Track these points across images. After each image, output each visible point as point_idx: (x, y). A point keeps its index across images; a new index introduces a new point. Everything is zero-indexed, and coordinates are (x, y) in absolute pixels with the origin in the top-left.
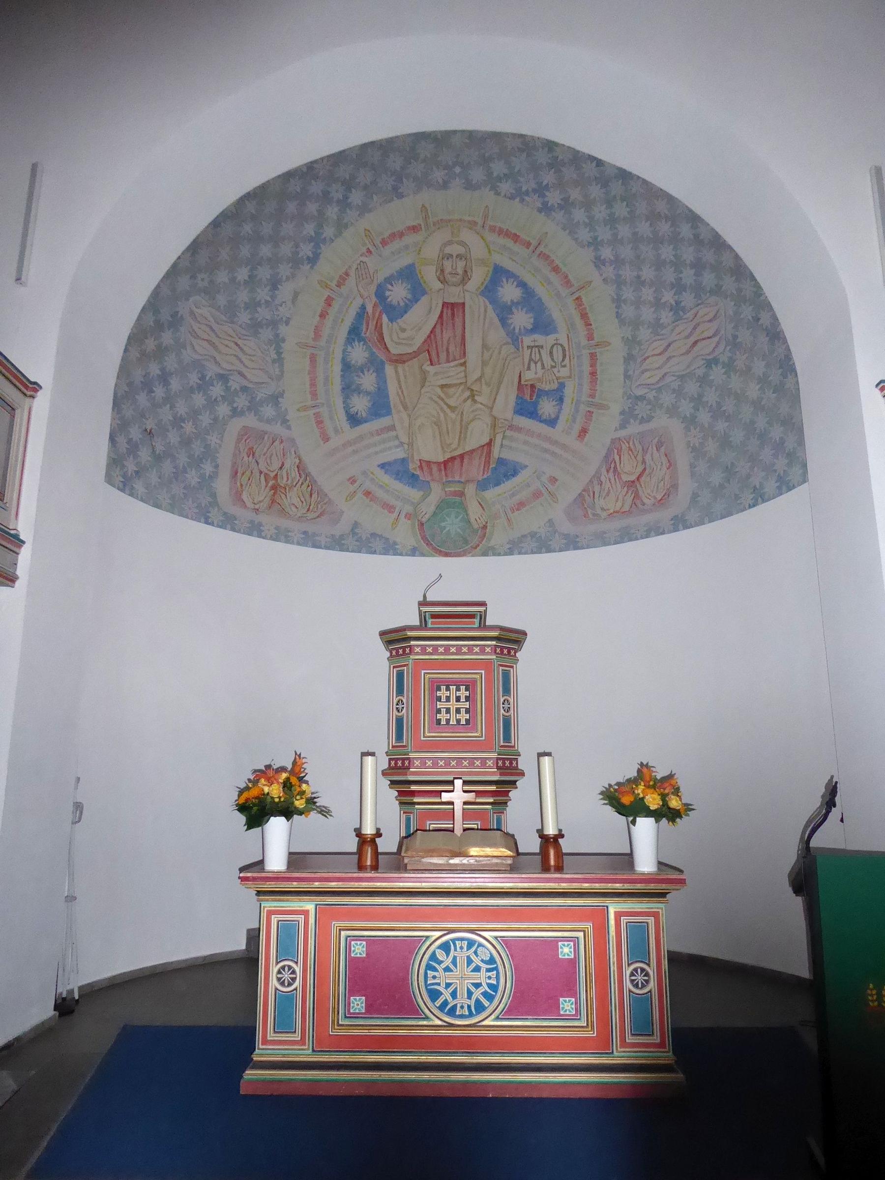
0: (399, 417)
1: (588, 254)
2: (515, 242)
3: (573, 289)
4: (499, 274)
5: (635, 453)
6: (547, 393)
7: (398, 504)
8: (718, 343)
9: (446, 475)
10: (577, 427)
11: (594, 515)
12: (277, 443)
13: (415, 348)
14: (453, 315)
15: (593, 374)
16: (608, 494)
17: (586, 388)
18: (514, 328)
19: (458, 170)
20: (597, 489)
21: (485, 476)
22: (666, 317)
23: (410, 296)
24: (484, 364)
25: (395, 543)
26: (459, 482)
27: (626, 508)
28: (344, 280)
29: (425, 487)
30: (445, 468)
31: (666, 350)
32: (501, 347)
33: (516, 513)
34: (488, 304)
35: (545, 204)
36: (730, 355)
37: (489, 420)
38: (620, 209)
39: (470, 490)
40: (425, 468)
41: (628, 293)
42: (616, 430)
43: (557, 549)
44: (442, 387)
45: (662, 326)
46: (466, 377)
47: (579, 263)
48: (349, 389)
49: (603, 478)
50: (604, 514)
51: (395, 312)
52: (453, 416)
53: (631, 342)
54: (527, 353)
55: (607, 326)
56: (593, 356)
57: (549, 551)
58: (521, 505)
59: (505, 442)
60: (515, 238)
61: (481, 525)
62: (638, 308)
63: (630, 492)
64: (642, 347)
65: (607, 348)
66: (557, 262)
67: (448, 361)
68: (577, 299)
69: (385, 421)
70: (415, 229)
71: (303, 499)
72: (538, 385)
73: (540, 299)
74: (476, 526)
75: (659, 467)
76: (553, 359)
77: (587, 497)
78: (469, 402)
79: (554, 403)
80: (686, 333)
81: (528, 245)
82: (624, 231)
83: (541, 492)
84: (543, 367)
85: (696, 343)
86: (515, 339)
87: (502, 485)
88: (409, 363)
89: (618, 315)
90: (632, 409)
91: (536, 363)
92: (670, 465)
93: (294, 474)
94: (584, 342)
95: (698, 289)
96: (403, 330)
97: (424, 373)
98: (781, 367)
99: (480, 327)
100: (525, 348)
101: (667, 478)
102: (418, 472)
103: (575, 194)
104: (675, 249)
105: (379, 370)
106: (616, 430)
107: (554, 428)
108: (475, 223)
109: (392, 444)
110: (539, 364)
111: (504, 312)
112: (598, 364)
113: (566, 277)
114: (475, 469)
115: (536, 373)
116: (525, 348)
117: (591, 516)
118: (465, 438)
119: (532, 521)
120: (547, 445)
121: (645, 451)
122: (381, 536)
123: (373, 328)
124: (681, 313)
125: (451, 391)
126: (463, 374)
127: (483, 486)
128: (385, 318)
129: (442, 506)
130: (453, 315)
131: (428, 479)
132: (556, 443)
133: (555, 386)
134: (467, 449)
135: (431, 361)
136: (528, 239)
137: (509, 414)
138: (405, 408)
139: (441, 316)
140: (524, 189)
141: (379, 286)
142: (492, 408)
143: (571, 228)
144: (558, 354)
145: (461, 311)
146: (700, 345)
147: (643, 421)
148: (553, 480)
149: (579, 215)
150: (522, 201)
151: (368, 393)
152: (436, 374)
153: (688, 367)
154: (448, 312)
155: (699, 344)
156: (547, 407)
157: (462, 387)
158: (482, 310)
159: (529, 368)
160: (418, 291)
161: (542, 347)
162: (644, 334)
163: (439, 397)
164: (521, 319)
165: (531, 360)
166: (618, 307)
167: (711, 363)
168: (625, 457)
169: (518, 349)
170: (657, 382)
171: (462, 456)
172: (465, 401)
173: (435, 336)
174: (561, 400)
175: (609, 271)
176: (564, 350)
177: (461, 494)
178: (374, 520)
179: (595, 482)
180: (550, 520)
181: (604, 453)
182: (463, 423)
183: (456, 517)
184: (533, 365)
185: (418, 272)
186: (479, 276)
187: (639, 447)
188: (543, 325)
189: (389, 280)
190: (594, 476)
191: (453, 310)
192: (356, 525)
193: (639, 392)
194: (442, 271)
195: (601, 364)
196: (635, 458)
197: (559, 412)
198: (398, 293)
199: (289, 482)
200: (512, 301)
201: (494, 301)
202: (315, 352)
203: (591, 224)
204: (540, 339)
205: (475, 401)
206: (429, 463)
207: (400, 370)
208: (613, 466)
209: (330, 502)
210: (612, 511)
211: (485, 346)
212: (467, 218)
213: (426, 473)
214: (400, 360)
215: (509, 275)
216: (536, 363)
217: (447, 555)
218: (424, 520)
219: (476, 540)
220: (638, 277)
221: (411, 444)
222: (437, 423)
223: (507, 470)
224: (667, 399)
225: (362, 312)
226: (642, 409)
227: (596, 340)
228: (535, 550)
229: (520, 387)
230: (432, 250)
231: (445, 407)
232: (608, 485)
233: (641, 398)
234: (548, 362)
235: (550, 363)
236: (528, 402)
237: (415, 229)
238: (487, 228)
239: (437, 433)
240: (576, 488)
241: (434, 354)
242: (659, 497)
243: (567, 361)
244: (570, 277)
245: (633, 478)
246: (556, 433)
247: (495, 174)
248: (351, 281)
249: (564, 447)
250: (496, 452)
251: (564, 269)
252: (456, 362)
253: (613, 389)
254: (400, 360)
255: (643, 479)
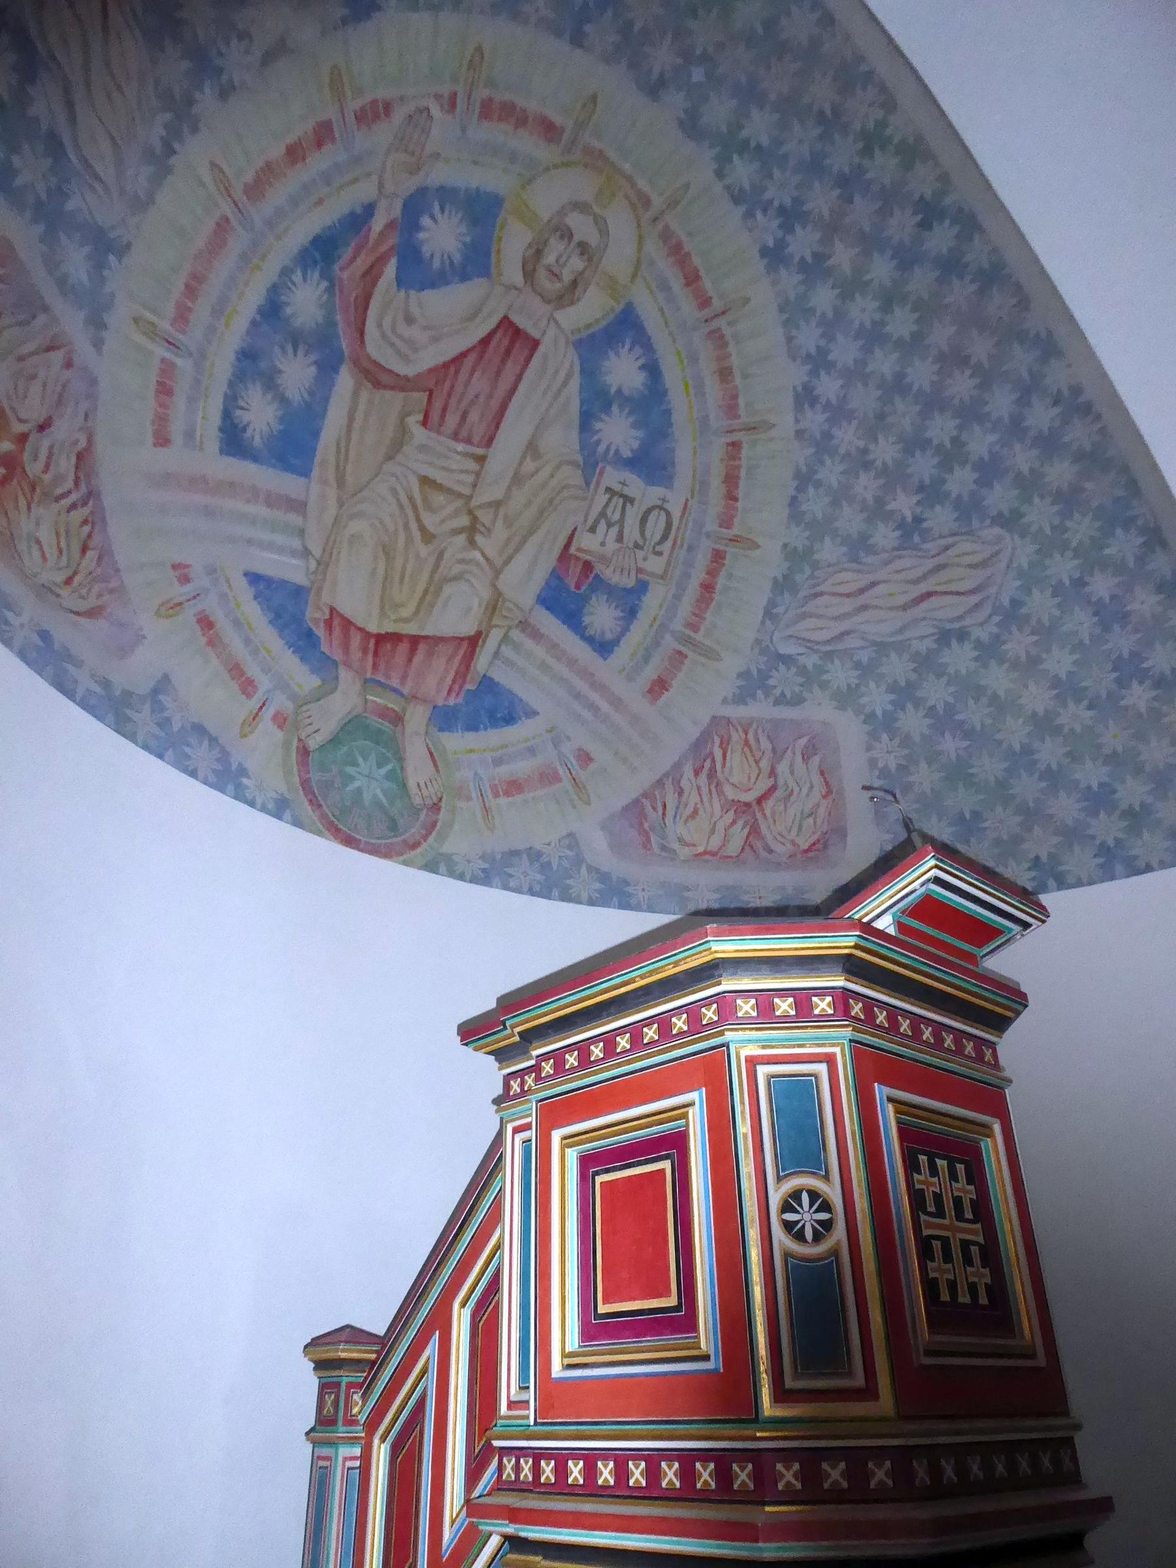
0: (316, 489)
1: (797, 375)
2: (688, 284)
3: (736, 423)
4: (625, 326)
5: (758, 754)
6: (612, 592)
7: (264, 683)
8: (977, 606)
9: (375, 666)
10: (650, 673)
11: (663, 848)
12: (57, 357)
13: (409, 371)
14: (508, 352)
15: (708, 588)
16: (695, 812)
17: (685, 609)
18: (598, 442)
19: (698, 74)
20: (671, 800)
21: (451, 702)
22: (885, 536)
23: (457, 258)
24: (517, 479)
25: (242, 771)
26: (395, 690)
27: (734, 847)
28: (376, 117)
29: (325, 666)
30: (376, 654)
31: (862, 591)
32: (558, 467)
33: (503, 801)
34: (577, 368)
35: (781, 245)
36: (995, 630)
37: (486, 594)
38: (901, 323)
39: (417, 717)
40: (337, 631)
41: (831, 473)
42: (725, 701)
43: (584, 896)
44: (425, 481)
45: (872, 550)
46: (474, 486)
47: (771, 383)
48: (251, 364)
49: (685, 784)
50: (684, 852)
51: (418, 272)
52: (424, 550)
53: (796, 557)
54: (603, 498)
55: (765, 516)
56: (718, 557)
57: (566, 897)
58: (514, 787)
59: (506, 651)
60: (692, 279)
61: (429, 802)
62: (835, 503)
63: (740, 823)
64: (817, 573)
65: (749, 552)
66: (735, 361)
67: (455, 436)
68: (733, 444)
69: (287, 484)
70: (549, 130)
71: (63, 545)
72: (599, 568)
73: (668, 413)
74: (417, 801)
75: (805, 790)
76: (642, 533)
77: (649, 809)
78: (461, 539)
79: (619, 614)
80: (913, 575)
81: (705, 302)
82: (884, 363)
83: (556, 772)
84: (620, 538)
85: (929, 594)
86: (591, 462)
87: (482, 733)
88: (388, 394)
89: (793, 502)
90: (764, 676)
91: (610, 525)
92: (829, 792)
93: (65, 465)
94: (711, 526)
95: (969, 510)
96: (410, 320)
97: (403, 431)
98: (1115, 669)
99: (542, 403)
100: (602, 489)
101: (822, 811)
102: (320, 632)
103: (843, 256)
104: (960, 428)
105: (328, 369)
106: (725, 701)
107: (605, 659)
108: (647, 203)
109: (279, 539)
110: (614, 531)
111: (597, 402)
112: (723, 573)
113: (735, 397)
114: (434, 677)
115: (603, 544)
116: (602, 489)
117: (656, 850)
118: (432, 605)
119: (535, 823)
120: (581, 685)
121: (778, 754)
122: (213, 740)
123: (363, 269)
124: (916, 539)
125: (439, 499)
126: (470, 479)
127: (444, 719)
128: (390, 270)
129: (352, 727)
130: (508, 352)
131: (338, 655)
132: (601, 688)
133: (630, 582)
134: (428, 631)
135: (426, 416)
136: (711, 293)
137: (527, 598)
138: (341, 482)
139: (485, 341)
140: (767, 195)
141: (422, 191)
142: (498, 573)
143: (794, 312)
144: (656, 525)
145: (526, 352)
146: (934, 601)
147: (780, 701)
148: (585, 758)
149: (824, 298)
150: (749, 215)
151: (283, 400)
152: (423, 448)
153: (901, 631)
154: (501, 341)
155: (933, 599)
156: (602, 616)
157: (459, 503)
158: (562, 375)
159: (593, 530)
160: (477, 261)
161: (632, 501)
162: (828, 551)
163: (411, 499)
164: (619, 432)
165: (603, 514)
166: (799, 489)
167: (944, 637)
168: (735, 759)
169: (588, 484)
170: (828, 642)
171: (415, 641)
172: (457, 532)
173: (457, 373)
174: (631, 613)
175: (815, 420)
176: (669, 524)
177: (397, 719)
178: (204, 692)
179: (668, 784)
180: (570, 835)
181: (694, 733)
182: (437, 577)
183: (379, 766)
184: (602, 526)
185: (499, 220)
186: (591, 308)
187: (765, 744)
188: (651, 462)
189: (446, 194)
190: (666, 775)
191: (512, 341)
192: (164, 684)
193: (785, 649)
194: (539, 253)
195: (730, 576)
196: (757, 762)
197: (623, 634)
198: (442, 236)
199: (47, 477)
200: (619, 392)
201: (590, 372)
202: (234, 222)
203: (831, 325)
204: (635, 485)
205: (472, 543)
206: (347, 624)
207: (364, 395)
208: (708, 764)
209: (119, 591)
210: (701, 849)
211: (532, 448)
212: (642, 184)
213: (335, 642)
214: (374, 376)
215: (643, 341)
216: (610, 525)
217: (349, 841)
218: (312, 744)
219: (415, 831)
220: (865, 451)
221: (324, 564)
222: (387, 552)
223: (492, 707)
224: (841, 675)
225: (358, 220)
226: (783, 679)
227: (736, 531)
228: (537, 888)
229: (565, 556)
230: (547, 199)
231: (414, 526)
232: (694, 798)
233: (787, 660)
234: (632, 532)
235: (636, 536)
236: (571, 589)
237: (549, 130)
238: (660, 226)
239: (381, 570)
240: (632, 786)
241: (438, 405)
242: (806, 846)
243: (667, 547)
244: (741, 401)
245: (750, 797)
246: (608, 670)
247: (744, 134)
248: (383, 134)
249: (616, 702)
250: (482, 662)
251: (738, 380)
252: (470, 449)
253: (738, 623)
254: (374, 376)
255: (769, 805)
